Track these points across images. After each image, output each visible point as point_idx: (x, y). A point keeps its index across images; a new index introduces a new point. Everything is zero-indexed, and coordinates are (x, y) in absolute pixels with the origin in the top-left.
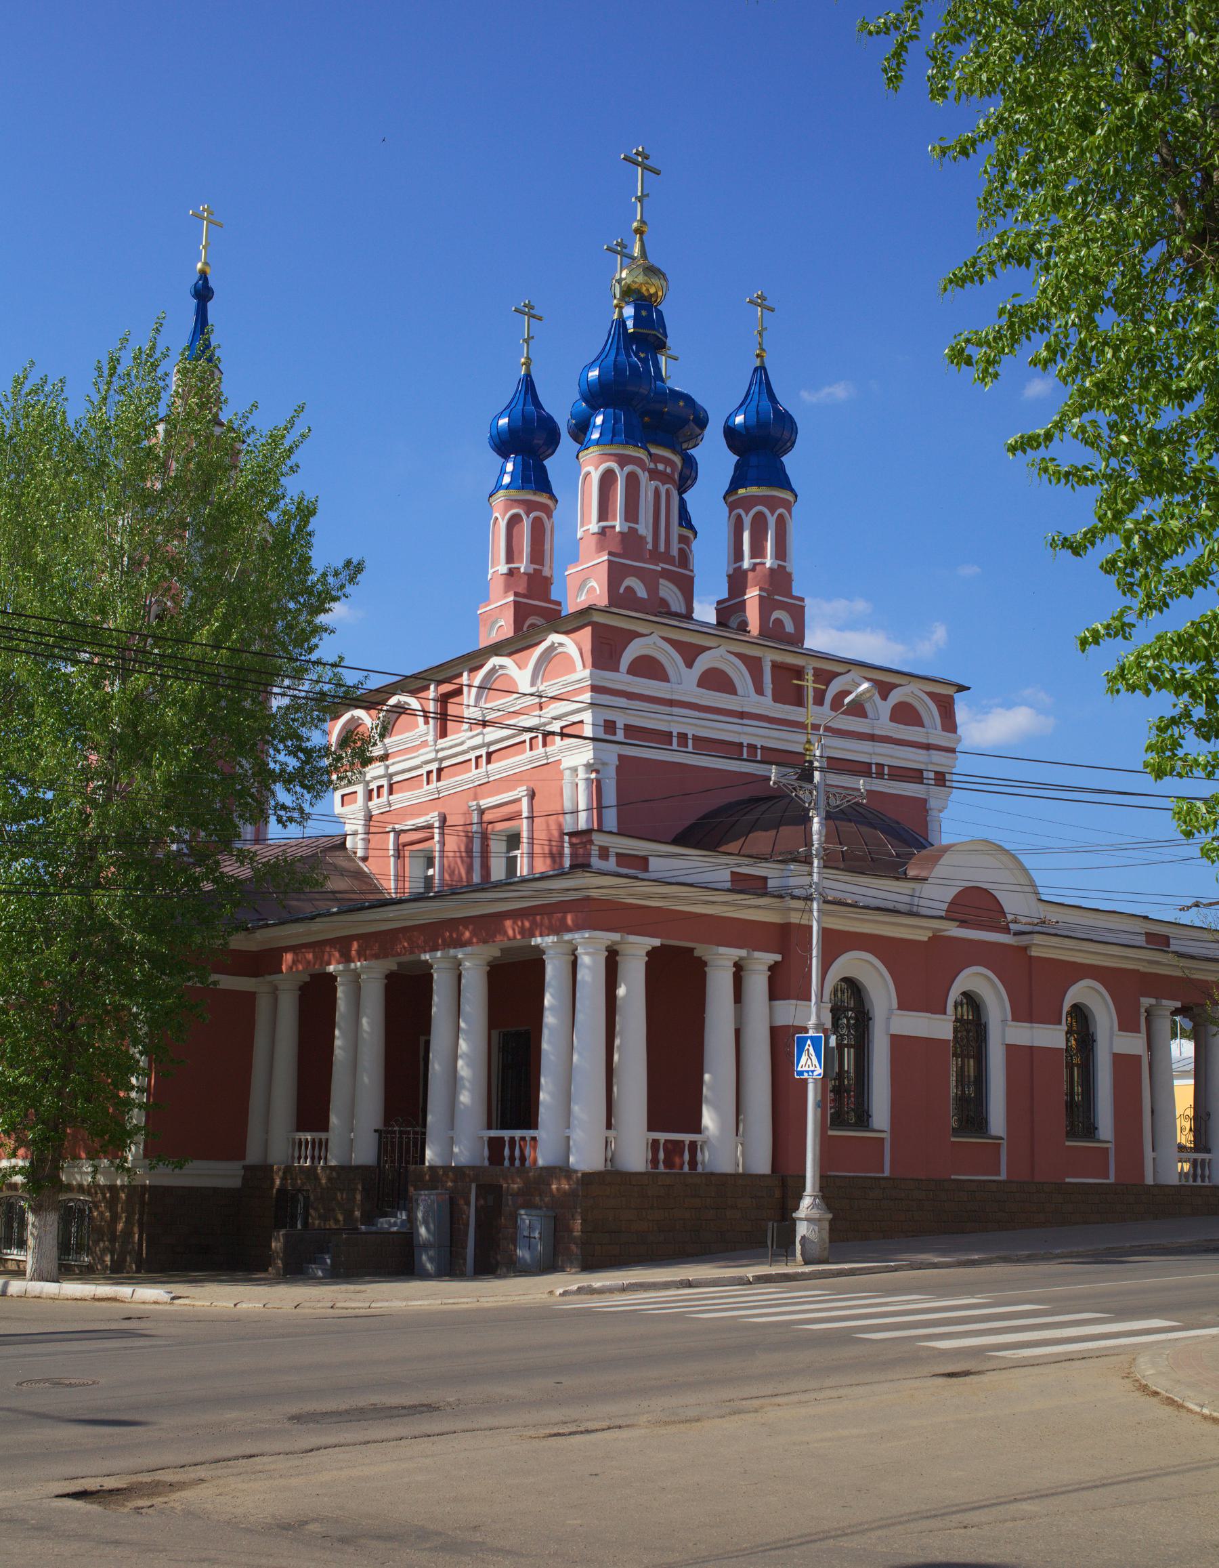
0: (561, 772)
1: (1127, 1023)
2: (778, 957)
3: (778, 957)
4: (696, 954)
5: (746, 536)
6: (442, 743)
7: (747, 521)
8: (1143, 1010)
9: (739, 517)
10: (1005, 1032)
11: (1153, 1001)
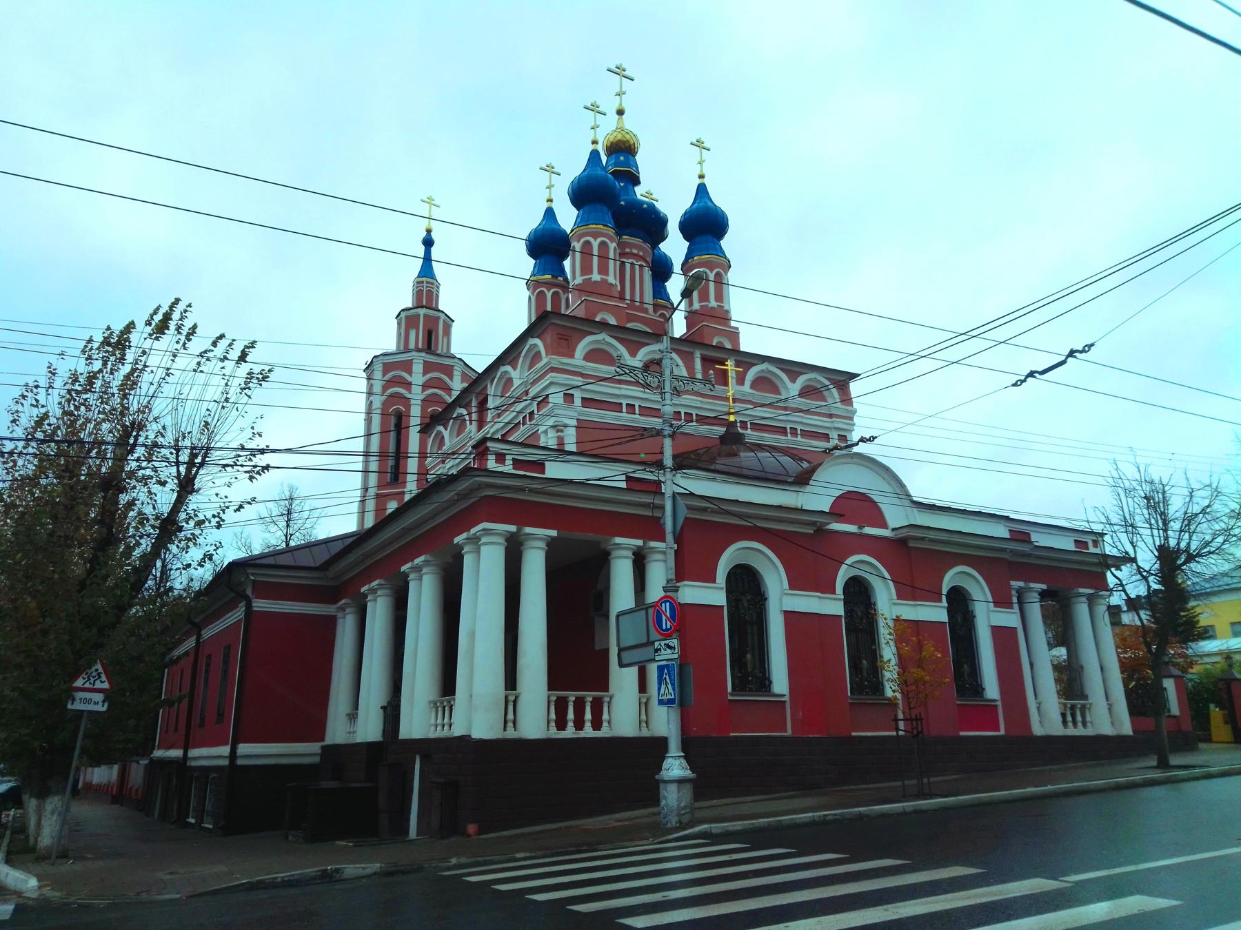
1: (1001, 601)
8: (1014, 592)
11: (1021, 584)
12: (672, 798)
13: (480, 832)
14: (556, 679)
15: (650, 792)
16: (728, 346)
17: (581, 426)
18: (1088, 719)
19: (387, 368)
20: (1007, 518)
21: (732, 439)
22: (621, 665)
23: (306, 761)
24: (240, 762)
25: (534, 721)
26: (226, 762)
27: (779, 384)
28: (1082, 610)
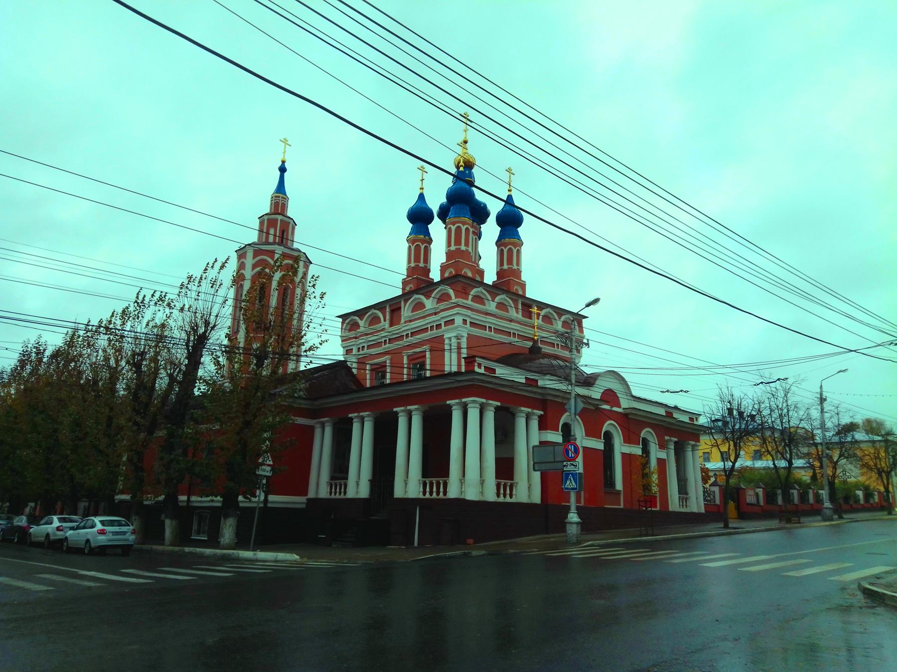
0: (444, 340)
2: (542, 413)
3: (542, 413)
5: (274, 302)
7: (505, 251)
9: (450, 228)
10: (620, 448)
12: (573, 530)
13: (475, 543)
14: (498, 476)
16: (521, 293)
17: (470, 337)
18: (514, 492)
19: (257, 253)
21: (535, 351)
22: (535, 470)
24: (269, 505)
25: (490, 495)
26: (262, 505)
28: (689, 454)
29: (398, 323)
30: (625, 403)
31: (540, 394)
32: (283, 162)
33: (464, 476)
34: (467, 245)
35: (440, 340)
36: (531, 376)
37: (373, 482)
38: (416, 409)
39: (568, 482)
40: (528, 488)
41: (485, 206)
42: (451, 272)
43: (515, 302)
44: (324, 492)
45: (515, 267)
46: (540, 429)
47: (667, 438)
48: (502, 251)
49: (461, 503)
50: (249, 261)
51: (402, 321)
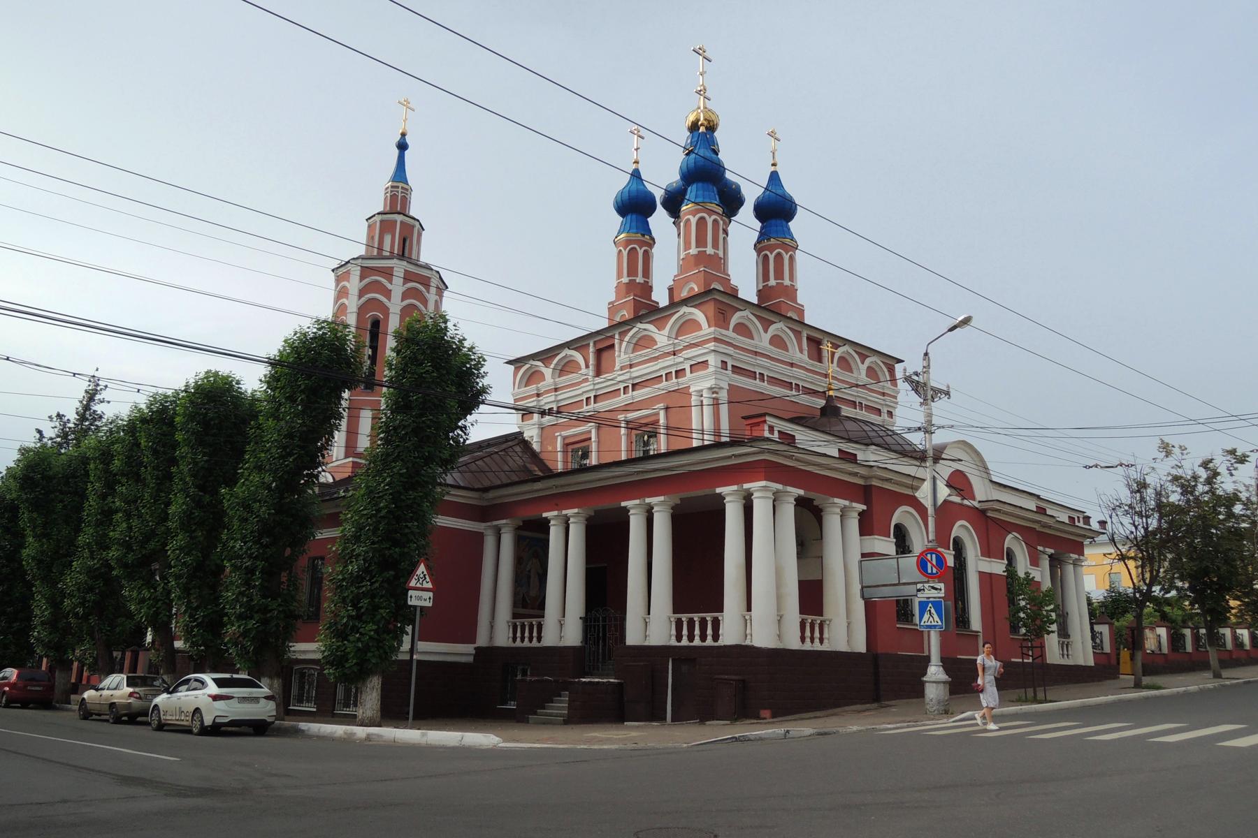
2: (865, 507)
3: (865, 507)
4: (815, 503)
6: (598, 380)
7: (771, 257)
14: (803, 610)
15: (917, 690)
17: (732, 389)
18: (826, 635)
19: (365, 272)
20: (1038, 497)
23: (463, 659)
25: (793, 643)
27: (880, 373)
29: (611, 370)
30: (982, 492)
31: (862, 477)
32: (403, 135)
33: (749, 609)
34: (715, 246)
35: (684, 392)
36: (850, 448)
37: (589, 622)
38: (661, 503)
39: (926, 616)
40: (846, 631)
41: (738, 188)
42: (692, 289)
43: (798, 334)
44: (503, 639)
45: (787, 282)
46: (861, 534)
47: (1040, 548)
48: (766, 258)
49: (744, 654)
50: (354, 284)
51: (617, 367)
